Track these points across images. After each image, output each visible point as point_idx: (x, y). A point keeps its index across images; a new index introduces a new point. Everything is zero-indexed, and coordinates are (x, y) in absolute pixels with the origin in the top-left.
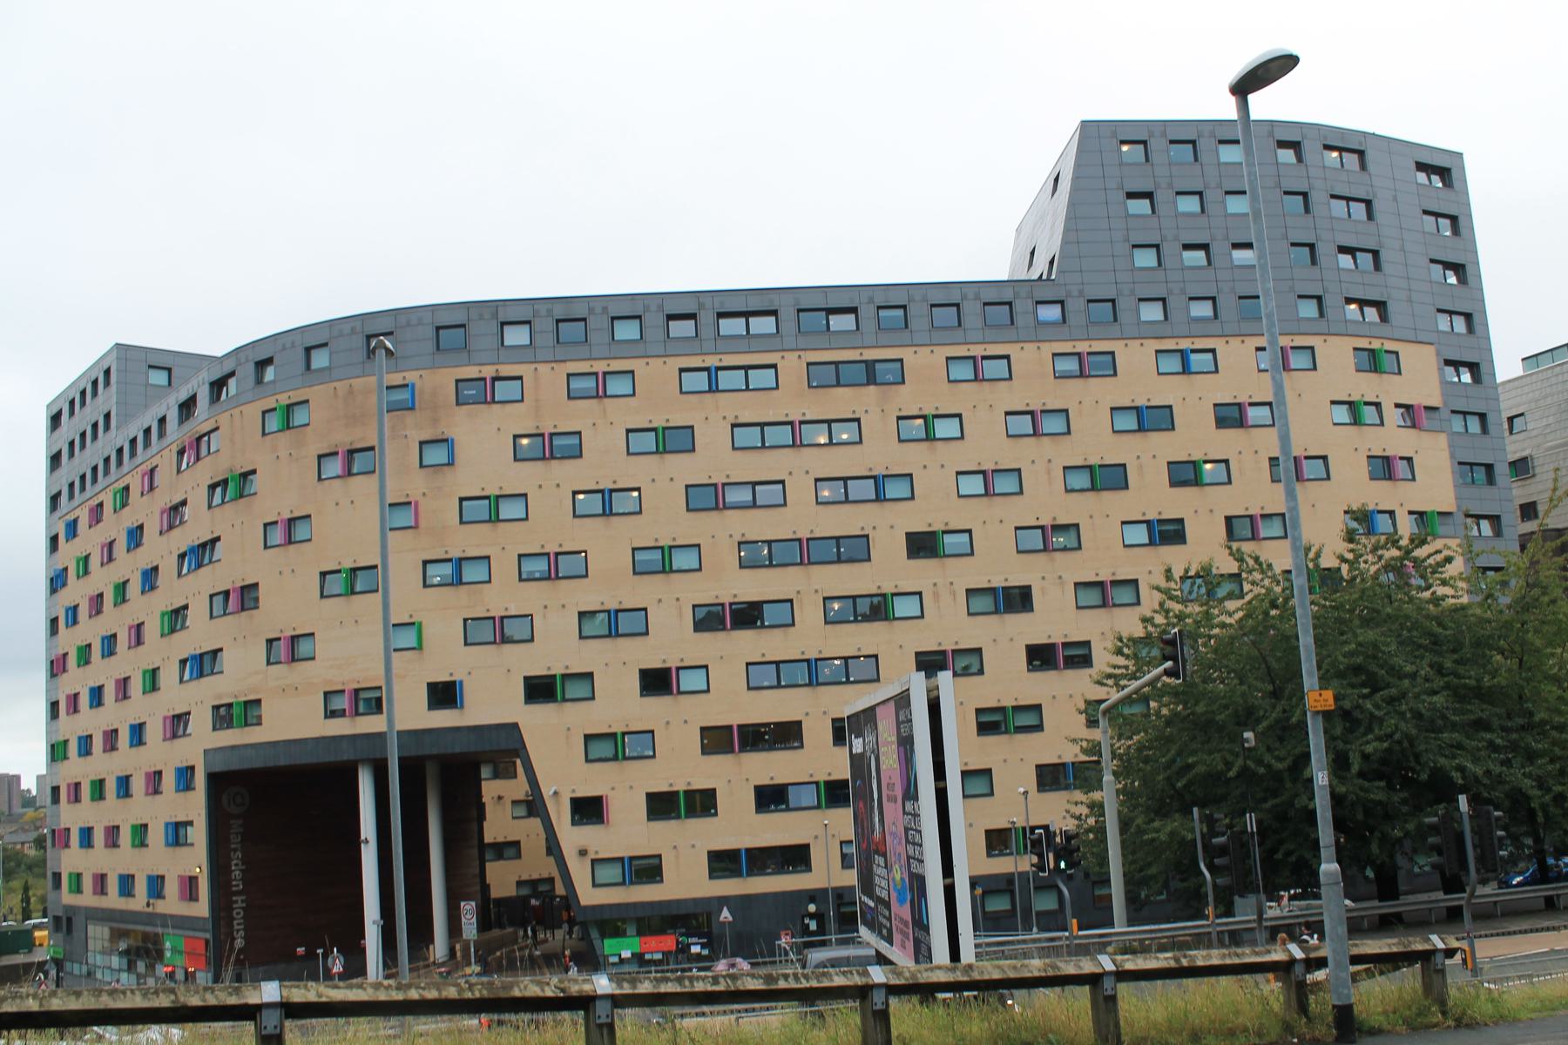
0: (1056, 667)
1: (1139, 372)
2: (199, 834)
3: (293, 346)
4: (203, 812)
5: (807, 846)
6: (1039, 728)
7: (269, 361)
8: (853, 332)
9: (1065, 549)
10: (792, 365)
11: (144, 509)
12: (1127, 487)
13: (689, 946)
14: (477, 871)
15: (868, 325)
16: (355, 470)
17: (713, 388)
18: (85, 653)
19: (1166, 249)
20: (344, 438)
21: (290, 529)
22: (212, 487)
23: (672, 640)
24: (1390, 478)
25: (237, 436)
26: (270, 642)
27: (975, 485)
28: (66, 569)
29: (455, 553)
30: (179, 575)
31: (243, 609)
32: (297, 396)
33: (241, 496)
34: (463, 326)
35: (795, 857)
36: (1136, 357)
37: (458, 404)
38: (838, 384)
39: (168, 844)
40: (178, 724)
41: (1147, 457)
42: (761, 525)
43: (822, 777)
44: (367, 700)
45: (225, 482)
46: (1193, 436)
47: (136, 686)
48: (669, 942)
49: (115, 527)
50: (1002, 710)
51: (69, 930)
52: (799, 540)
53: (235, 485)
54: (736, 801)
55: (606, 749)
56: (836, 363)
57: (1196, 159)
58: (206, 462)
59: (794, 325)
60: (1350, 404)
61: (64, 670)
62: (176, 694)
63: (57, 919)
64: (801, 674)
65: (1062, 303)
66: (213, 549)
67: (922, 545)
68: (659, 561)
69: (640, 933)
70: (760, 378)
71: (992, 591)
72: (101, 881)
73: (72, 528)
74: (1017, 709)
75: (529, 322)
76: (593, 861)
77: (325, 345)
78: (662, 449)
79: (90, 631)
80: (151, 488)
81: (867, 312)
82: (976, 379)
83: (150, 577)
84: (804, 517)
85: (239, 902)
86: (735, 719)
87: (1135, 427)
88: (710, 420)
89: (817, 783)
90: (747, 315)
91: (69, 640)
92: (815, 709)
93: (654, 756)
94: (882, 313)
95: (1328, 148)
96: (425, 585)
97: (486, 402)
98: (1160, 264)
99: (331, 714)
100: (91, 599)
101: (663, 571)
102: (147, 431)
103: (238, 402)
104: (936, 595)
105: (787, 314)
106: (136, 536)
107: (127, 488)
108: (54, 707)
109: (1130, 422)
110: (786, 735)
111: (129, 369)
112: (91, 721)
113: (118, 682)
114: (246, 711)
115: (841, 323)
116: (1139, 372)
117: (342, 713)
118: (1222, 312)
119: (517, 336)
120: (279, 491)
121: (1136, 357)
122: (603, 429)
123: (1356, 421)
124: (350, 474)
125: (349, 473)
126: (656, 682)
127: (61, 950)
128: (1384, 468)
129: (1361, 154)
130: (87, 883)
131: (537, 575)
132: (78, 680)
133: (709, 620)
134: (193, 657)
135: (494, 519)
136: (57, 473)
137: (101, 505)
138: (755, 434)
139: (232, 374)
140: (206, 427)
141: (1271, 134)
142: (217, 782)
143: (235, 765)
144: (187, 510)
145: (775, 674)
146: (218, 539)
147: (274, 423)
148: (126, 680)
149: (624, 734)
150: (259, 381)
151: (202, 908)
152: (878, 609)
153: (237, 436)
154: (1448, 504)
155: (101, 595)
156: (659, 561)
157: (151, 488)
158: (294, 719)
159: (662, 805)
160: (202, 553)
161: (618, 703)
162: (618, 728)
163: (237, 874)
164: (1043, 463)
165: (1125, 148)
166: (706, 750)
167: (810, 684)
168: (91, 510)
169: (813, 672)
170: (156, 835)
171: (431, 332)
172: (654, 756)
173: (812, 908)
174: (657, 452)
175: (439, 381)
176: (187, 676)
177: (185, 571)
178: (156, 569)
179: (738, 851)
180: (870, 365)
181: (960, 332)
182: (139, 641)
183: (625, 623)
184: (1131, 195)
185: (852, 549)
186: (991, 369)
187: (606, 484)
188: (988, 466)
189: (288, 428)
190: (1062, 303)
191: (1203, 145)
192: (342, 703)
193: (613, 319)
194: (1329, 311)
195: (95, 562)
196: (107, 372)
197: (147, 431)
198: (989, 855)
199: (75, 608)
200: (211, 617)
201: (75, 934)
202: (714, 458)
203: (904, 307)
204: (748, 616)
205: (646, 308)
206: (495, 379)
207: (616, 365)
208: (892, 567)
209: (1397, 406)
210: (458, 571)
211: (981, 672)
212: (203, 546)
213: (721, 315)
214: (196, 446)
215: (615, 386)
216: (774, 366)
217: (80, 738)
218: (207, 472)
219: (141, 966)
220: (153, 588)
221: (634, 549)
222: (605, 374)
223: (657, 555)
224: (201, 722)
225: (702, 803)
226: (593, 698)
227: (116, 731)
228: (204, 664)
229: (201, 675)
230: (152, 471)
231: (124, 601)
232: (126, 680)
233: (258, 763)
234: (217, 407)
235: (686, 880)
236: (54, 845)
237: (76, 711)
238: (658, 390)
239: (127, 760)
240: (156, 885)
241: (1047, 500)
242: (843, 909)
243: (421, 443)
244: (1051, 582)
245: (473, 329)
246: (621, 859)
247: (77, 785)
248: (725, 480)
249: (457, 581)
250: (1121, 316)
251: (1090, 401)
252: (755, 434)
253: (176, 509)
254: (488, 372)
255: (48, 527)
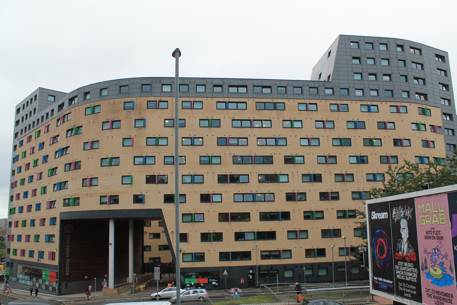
0: (328, 200)
1: (356, 111)
2: (57, 239)
3: (96, 88)
4: (58, 232)
5: (250, 252)
6: (322, 218)
7: (88, 93)
8: (270, 93)
9: (332, 163)
10: (251, 102)
11: (46, 138)
12: (351, 145)
13: (212, 282)
14: (141, 255)
15: (274, 92)
16: (114, 127)
17: (227, 108)
18: (23, 181)
19: (364, 74)
20: (111, 117)
21: (92, 145)
22: (68, 131)
23: (211, 185)
24: (428, 147)
25: (77, 115)
26: (84, 179)
27: (305, 142)
28: (18, 155)
29: (144, 155)
30: (55, 158)
31: (75, 169)
32: (97, 104)
33: (77, 134)
34: (150, 85)
35: (246, 255)
36: (354, 106)
37: (148, 108)
38: (265, 109)
39: (46, 242)
40: (51, 204)
41: (357, 137)
42: (240, 151)
43: (256, 230)
44: (113, 199)
45: (72, 129)
46: (372, 131)
47: (39, 192)
48: (206, 280)
49: (35, 143)
50: (311, 212)
51: (12, 267)
52: (251, 156)
53: (76, 130)
54: (229, 237)
55: (189, 218)
56: (265, 103)
57: (373, 48)
58: (66, 123)
59: (252, 90)
60: (417, 124)
61: (16, 186)
62: (51, 195)
63: (8, 263)
64: (250, 198)
65: (333, 89)
66: (67, 150)
67: (289, 160)
68: (207, 160)
69: (197, 277)
70: (241, 106)
71: (310, 175)
72: (31, 253)
73: (21, 143)
74: (316, 212)
75: (171, 85)
76: (183, 254)
77: (107, 88)
78: (210, 126)
79: (25, 174)
80: (48, 131)
81: (274, 88)
82: (307, 110)
83: (46, 158)
84: (253, 149)
85: (68, 261)
86: (229, 211)
87: (354, 127)
88: (226, 118)
89: (254, 232)
90: (238, 86)
91: (18, 177)
92: (255, 209)
93: (204, 222)
94: (279, 88)
95: (411, 48)
96: (134, 164)
97: (156, 108)
98: (362, 79)
99: (102, 203)
100: (26, 165)
101: (209, 164)
102: (43, 117)
103: (78, 105)
104: (293, 175)
105: (250, 87)
106: (42, 145)
107: (40, 131)
108: (12, 198)
109: (352, 126)
110: (245, 217)
111: (43, 95)
112: (23, 202)
113: (33, 190)
114: (76, 201)
115: (265, 90)
116: (356, 111)
117: (106, 203)
118: (380, 94)
119: (167, 89)
120: (88, 134)
121: (354, 106)
122: (192, 119)
123: (419, 129)
124: (112, 128)
125: (112, 128)
126: (206, 198)
127: (8, 273)
128: (427, 144)
129: (420, 50)
130: (19, 252)
131: (170, 163)
132: (20, 189)
133: (222, 179)
134: (58, 183)
135: (157, 145)
136: (18, 126)
137: (31, 136)
138: (240, 123)
139: (76, 96)
140: (67, 112)
141: (395, 42)
142: (64, 223)
143: (70, 218)
144: (59, 138)
145: (243, 197)
146: (69, 147)
147: (89, 111)
148: (36, 190)
149: (195, 214)
150: (85, 99)
151: (56, 262)
152: (272, 178)
153: (77, 115)
154: (444, 156)
155: (29, 164)
156: (207, 160)
157: (48, 131)
158: (90, 204)
159: (205, 237)
160: (63, 151)
161: (193, 205)
162: (193, 212)
163: (68, 252)
164: (326, 137)
165: (352, 44)
166: (220, 220)
167: (253, 201)
168: (28, 138)
169: (254, 198)
170: (42, 238)
171: (140, 86)
172: (204, 222)
173: (251, 271)
174: (209, 127)
175: (142, 101)
176: (55, 189)
177: (57, 156)
178: (48, 156)
179: (229, 252)
180: (275, 104)
181: (302, 96)
182: (41, 178)
183: (197, 179)
184: (354, 58)
185: (268, 160)
186: (311, 107)
187: (193, 136)
188: (310, 137)
189: (94, 113)
190: (333, 89)
191: (375, 44)
192: (106, 200)
193: (197, 85)
194: (411, 96)
195: (28, 154)
196: (36, 96)
197: (47, 114)
198: (306, 257)
199: (21, 167)
200: (65, 171)
201: (13, 268)
202: (226, 130)
203: (285, 87)
204: (234, 179)
205: (207, 83)
206: (160, 101)
207: (197, 99)
208: (278, 167)
209: (430, 125)
210: (145, 160)
211: (305, 200)
212: (64, 149)
213: (230, 86)
214: (63, 118)
215: (197, 106)
216: (246, 103)
217: (19, 207)
218: (66, 126)
219: (34, 279)
220: (46, 162)
221: (200, 156)
222: (194, 102)
223: (207, 159)
224: (59, 205)
225: (218, 237)
226: (185, 202)
227: (31, 205)
228: (62, 185)
229: (60, 189)
230: (48, 126)
231: (37, 165)
232: (36, 190)
233: (77, 218)
234: (71, 106)
235: (212, 261)
236: (9, 240)
237: (19, 199)
238: (210, 107)
239: (34, 215)
240: (41, 254)
241: (327, 148)
242: (260, 272)
243: (135, 120)
244: (328, 173)
245: (153, 85)
246: (192, 253)
247: (17, 222)
248: (229, 137)
249: (145, 163)
250: (350, 93)
251: (341, 119)
252: (240, 123)
253: (55, 138)
254: (158, 99)
255: (14, 143)
